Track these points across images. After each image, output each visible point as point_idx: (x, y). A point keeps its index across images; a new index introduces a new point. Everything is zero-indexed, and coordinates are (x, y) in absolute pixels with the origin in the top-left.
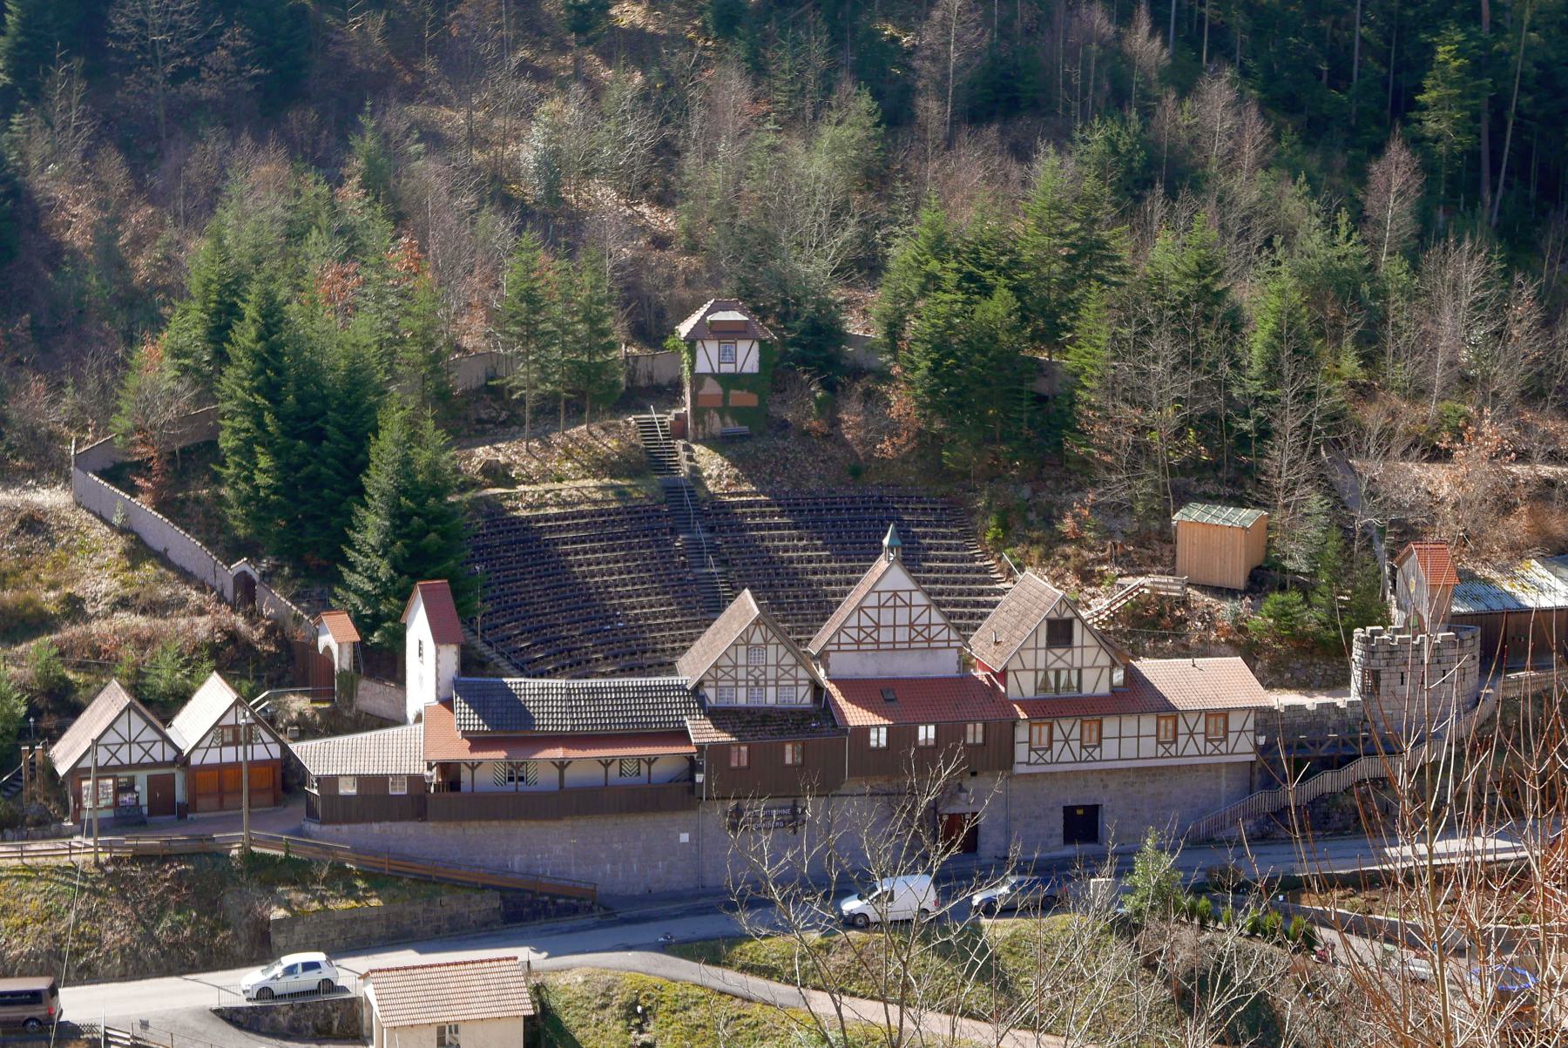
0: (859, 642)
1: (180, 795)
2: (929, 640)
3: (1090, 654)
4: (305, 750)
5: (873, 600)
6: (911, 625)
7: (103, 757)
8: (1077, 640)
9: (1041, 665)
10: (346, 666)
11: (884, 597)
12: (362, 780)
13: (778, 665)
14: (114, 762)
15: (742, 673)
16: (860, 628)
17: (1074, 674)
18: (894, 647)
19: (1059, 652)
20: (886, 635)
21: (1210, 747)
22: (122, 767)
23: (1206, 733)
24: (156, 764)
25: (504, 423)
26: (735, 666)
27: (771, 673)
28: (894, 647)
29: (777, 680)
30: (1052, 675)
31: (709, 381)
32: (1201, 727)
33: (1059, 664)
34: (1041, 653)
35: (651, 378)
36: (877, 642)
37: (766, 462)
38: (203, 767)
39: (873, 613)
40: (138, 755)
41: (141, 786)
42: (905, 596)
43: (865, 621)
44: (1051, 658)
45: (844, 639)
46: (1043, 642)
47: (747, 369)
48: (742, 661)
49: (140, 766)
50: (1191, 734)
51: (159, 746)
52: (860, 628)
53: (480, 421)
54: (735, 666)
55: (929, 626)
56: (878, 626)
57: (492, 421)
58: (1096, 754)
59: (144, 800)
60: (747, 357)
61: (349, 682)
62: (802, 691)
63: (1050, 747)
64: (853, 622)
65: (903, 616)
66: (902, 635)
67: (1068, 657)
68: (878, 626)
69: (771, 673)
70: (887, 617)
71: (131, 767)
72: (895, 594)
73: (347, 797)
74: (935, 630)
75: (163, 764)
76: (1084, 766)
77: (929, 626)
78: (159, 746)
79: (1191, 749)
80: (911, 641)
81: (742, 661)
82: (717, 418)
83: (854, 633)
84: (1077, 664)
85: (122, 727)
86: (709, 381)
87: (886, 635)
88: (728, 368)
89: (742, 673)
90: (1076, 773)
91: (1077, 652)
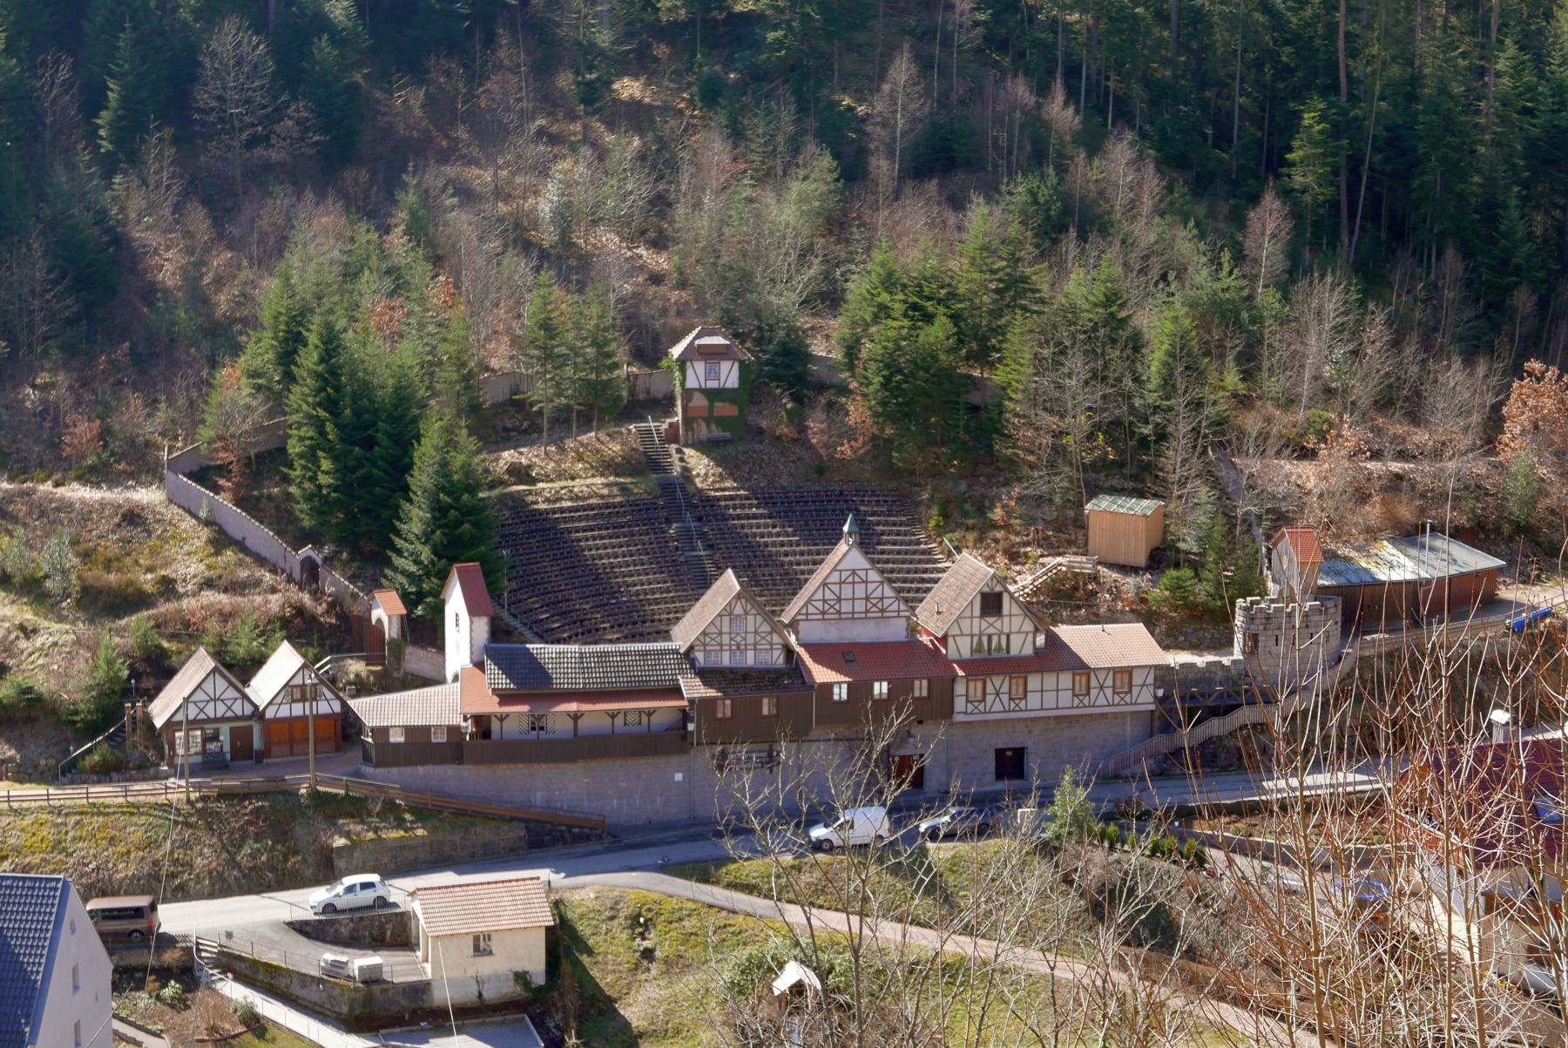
0: (824, 613)
1: (257, 743)
2: (882, 611)
3: (1017, 622)
5: (835, 577)
6: (867, 598)
7: (193, 712)
9: (976, 631)
11: (845, 575)
13: (756, 632)
14: (202, 716)
15: (726, 639)
16: (825, 601)
17: (1004, 639)
18: (853, 616)
19: (991, 620)
21: (1117, 699)
22: (209, 720)
24: (236, 718)
25: (526, 432)
26: (721, 633)
28: (853, 616)
29: (755, 644)
30: (985, 640)
31: (697, 395)
33: (991, 630)
34: (976, 621)
35: (648, 392)
36: (839, 612)
37: (746, 463)
38: (275, 720)
39: (835, 588)
40: (221, 710)
41: (225, 737)
43: (829, 595)
44: (984, 625)
45: (811, 609)
46: (977, 612)
47: (728, 385)
48: (726, 629)
49: (224, 719)
52: (825, 601)
53: (505, 429)
54: (721, 633)
55: (882, 599)
56: (839, 600)
57: (514, 429)
58: (1022, 705)
59: (227, 748)
60: (729, 375)
61: (397, 648)
62: (776, 653)
64: (819, 595)
65: (860, 591)
66: (860, 606)
67: (998, 624)
68: (839, 600)
70: (847, 592)
71: (216, 720)
72: (854, 572)
77: (882, 599)
79: (1101, 701)
80: (867, 611)
81: (726, 629)
82: (704, 425)
83: (819, 605)
84: (1006, 630)
85: (208, 686)
86: (697, 395)
87: (846, 607)
88: (712, 384)
89: (726, 639)
91: (1006, 620)
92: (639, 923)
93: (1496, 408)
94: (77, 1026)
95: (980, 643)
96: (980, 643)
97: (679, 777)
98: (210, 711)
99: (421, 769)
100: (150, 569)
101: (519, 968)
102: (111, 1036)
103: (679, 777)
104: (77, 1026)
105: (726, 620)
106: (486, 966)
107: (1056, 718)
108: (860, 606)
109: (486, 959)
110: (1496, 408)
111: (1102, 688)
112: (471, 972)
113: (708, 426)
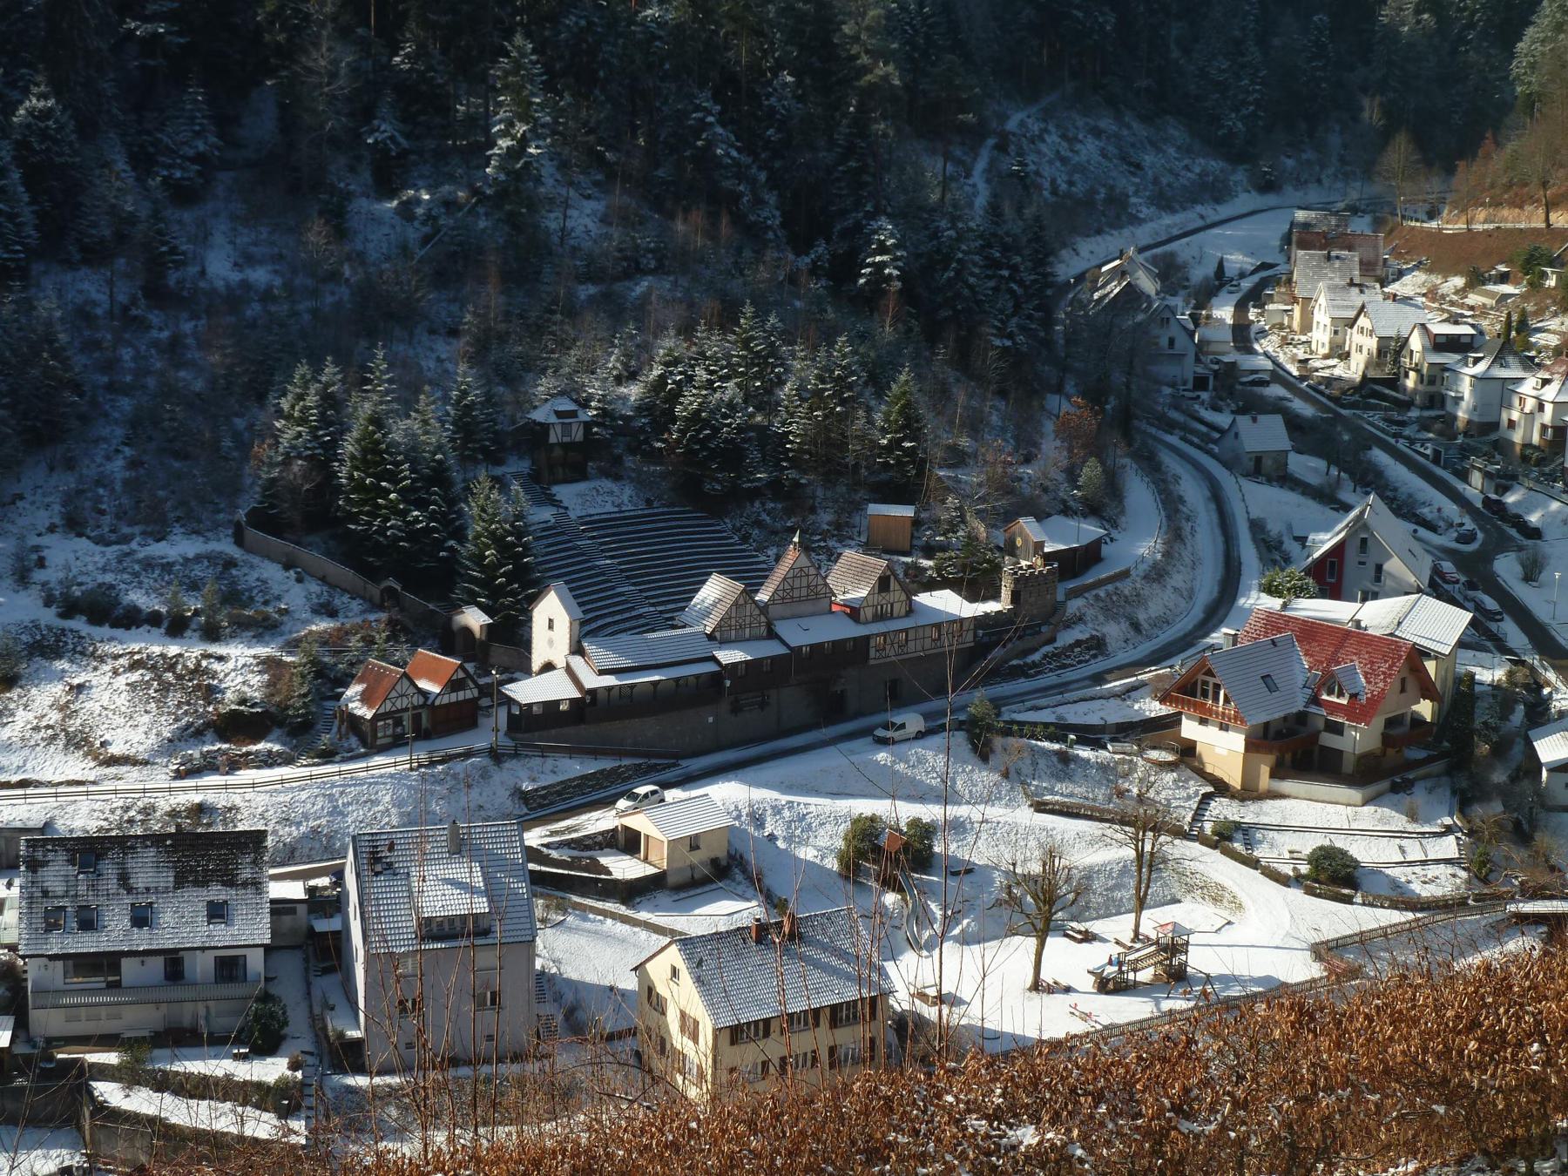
20: (796, 593)
38: (441, 706)
49: (406, 709)
65: (804, 584)
70: (797, 584)
73: (564, 712)
87: (796, 593)
88: (566, 439)
97: (711, 720)
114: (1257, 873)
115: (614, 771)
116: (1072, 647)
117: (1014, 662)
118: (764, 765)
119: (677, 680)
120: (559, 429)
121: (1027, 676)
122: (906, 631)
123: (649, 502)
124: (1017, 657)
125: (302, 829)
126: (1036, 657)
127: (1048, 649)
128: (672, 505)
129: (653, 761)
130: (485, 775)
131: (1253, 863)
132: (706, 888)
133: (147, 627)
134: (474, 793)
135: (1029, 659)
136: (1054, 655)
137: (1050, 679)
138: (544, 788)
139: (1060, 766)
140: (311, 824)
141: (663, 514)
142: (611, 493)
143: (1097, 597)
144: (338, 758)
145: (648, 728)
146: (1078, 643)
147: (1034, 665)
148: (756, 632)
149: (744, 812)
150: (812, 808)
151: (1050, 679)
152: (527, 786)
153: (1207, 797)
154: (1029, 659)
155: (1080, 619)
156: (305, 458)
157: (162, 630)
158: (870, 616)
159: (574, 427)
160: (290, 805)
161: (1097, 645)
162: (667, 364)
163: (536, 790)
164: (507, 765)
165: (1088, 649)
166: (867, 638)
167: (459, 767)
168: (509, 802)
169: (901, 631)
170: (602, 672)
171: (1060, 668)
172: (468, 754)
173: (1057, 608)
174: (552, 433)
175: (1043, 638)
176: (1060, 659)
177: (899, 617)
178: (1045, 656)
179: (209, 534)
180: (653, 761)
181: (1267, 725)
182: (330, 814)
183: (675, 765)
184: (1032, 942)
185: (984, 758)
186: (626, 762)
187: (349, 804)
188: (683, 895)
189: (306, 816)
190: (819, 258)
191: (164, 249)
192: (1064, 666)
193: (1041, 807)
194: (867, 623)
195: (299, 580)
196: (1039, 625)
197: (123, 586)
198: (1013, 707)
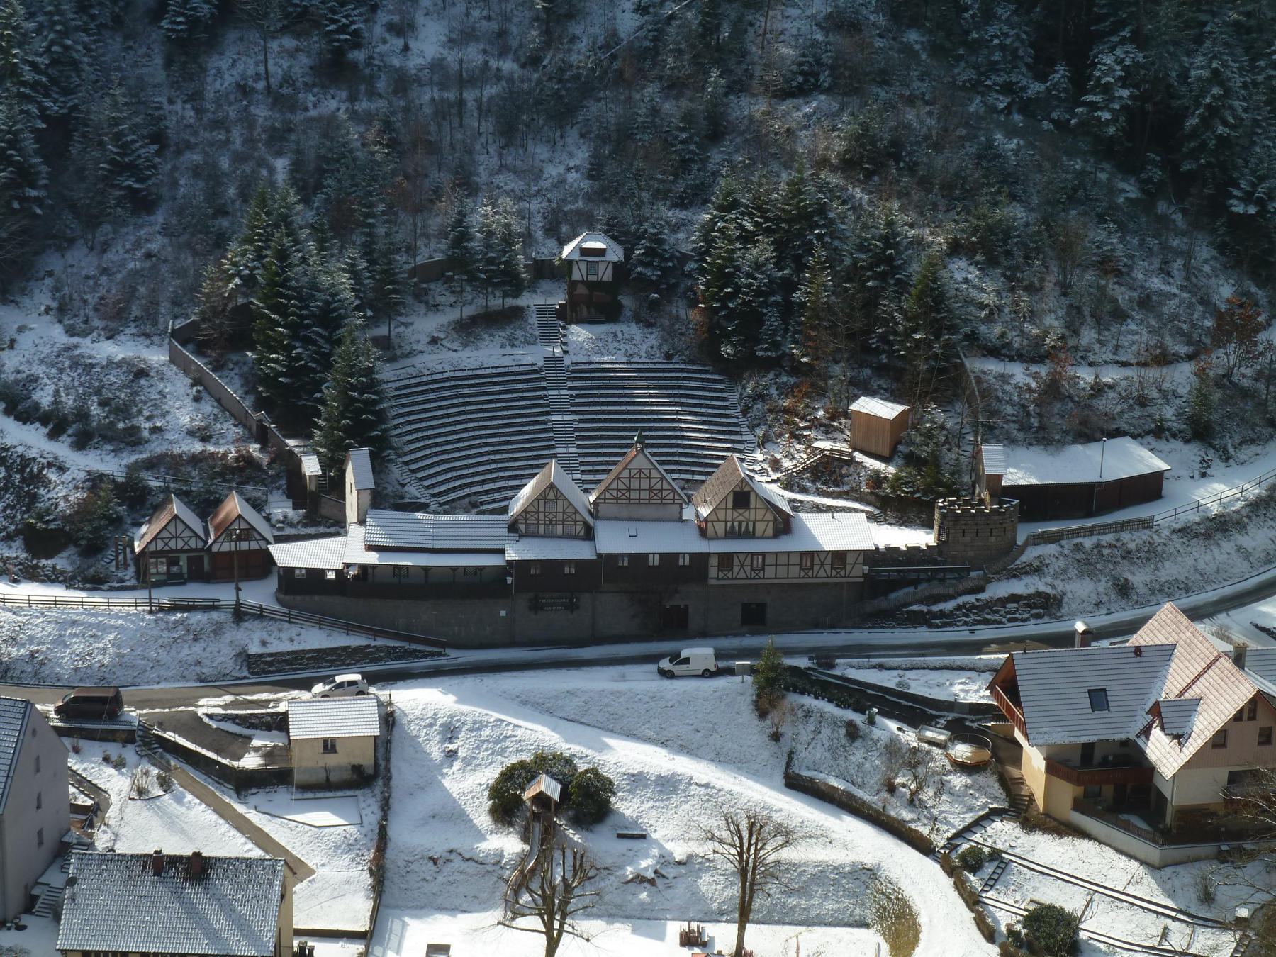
0: (617, 498)
1: (206, 566)
2: (662, 499)
3: (760, 514)
4: (275, 549)
5: (626, 474)
6: (650, 489)
7: (160, 545)
8: (752, 504)
9: (729, 518)
10: (313, 488)
11: (633, 472)
12: (663, 556)
13: (564, 513)
14: (166, 548)
15: (541, 516)
16: (618, 490)
17: (751, 525)
18: (639, 502)
19: (741, 511)
20: (634, 495)
21: (834, 573)
22: (172, 551)
23: (832, 565)
24: (191, 550)
26: (538, 512)
27: (560, 517)
28: (639, 502)
29: (563, 521)
30: (736, 524)
31: (580, 285)
32: (748, 562)
33: (741, 518)
34: (729, 512)
36: (629, 499)
38: (219, 553)
39: (626, 482)
40: (180, 544)
41: (183, 562)
42: (647, 472)
43: (621, 486)
44: (736, 514)
45: (608, 496)
46: (730, 505)
47: (605, 279)
48: (542, 509)
49: (182, 551)
50: (822, 564)
51: (193, 540)
52: (618, 490)
54: (538, 512)
55: (661, 490)
56: (629, 489)
58: (761, 574)
59: (185, 570)
62: (579, 528)
63: (812, 568)
64: (614, 486)
65: (645, 484)
66: (645, 495)
67: (746, 514)
68: (629, 489)
69: (560, 517)
70: (635, 484)
71: (177, 551)
72: (640, 470)
73: (330, 580)
74: (665, 493)
75: (196, 550)
76: (844, 580)
77: (661, 490)
78: (193, 540)
79: (822, 573)
80: (650, 499)
81: (542, 509)
82: (585, 310)
83: (614, 493)
84: (752, 518)
85: (171, 528)
86: (580, 285)
87: (634, 495)
88: (592, 278)
89: (541, 516)
90: (827, 584)
91: (753, 512)
92: (450, 732)
93: (1131, 365)
94: (38, 770)
95: (733, 526)
96: (733, 526)
97: (503, 613)
98: (172, 544)
99: (317, 598)
100: (149, 418)
101: (356, 761)
102: (69, 808)
103: (503, 613)
104: (38, 759)
105: (542, 503)
106: (332, 760)
107: (788, 584)
108: (645, 495)
109: (332, 755)
110: (1131, 365)
111: (822, 564)
112: (321, 764)
113: (588, 308)
114: (969, 916)
115: (358, 650)
116: (1003, 601)
117: (915, 608)
118: (515, 674)
119: (426, 569)
120: (583, 267)
121: (931, 626)
122: (763, 554)
123: (668, 357)
124: (921, 602)
125: (22, 651)
126: (949, 606)
127: (970, 599)
128: (692, 362)
129: (414, 646)
130: (218, 630)
131: (973, 901)
132: (340, 794)
133: (38, 425)
134: (197, 648)
135: (935, 608)
136: (974, 606)
137: (959, 634)
138: (270, 655)
139: (844, 741)
140: (33, 648)
141: (682, 370)
142: (631, 340)
143: (1078, 547)
144: (106, 586)
145: (426, 613)
146: (1014, 598)
147: (942, 614)
148: (570, 530)
149: (440, 721)
150: (519, 732)
151: (959, 634)
152: (255, 649)
153: (993, 814)
154: (935, 608)
155: (1037, 569)
156: (241, 278)
157: (47, 431)
158: (721, 531)
159: (602, 268)
160: (22, 626)
161: (1047, 604)
162: (721, 208)
163: (261, 656)
164: (246, 624)
165: (1030, 606)
166: (708, 555)
167: (197, 618)
168: (231, 663)
169: (758, 554)
170: (370, 548)
171: (979, 622)
172: (213, 607)
173: (1011, 550)
174: (575, 269)
175: (967, 584)
176: (984, 613)
177: (762, 537)
178: (959, 607)
179: (156, 339)
180: (414, 646)
181: (1088, 748)
182: (53, 642)
183: (439, 654)
184: (734, 928)
185: (763, 714)
186: (380, 642)
187: (75, 635)
188: (310, 795)
189: (31, 639)
190: (1054, 86)
191: (333, 27)
192: (987, 622)
193: (796, 784)
194: (717, 538)
195: (197, 399)
196: (969, 570)
197: (46, 380)
198: (855, 661)
